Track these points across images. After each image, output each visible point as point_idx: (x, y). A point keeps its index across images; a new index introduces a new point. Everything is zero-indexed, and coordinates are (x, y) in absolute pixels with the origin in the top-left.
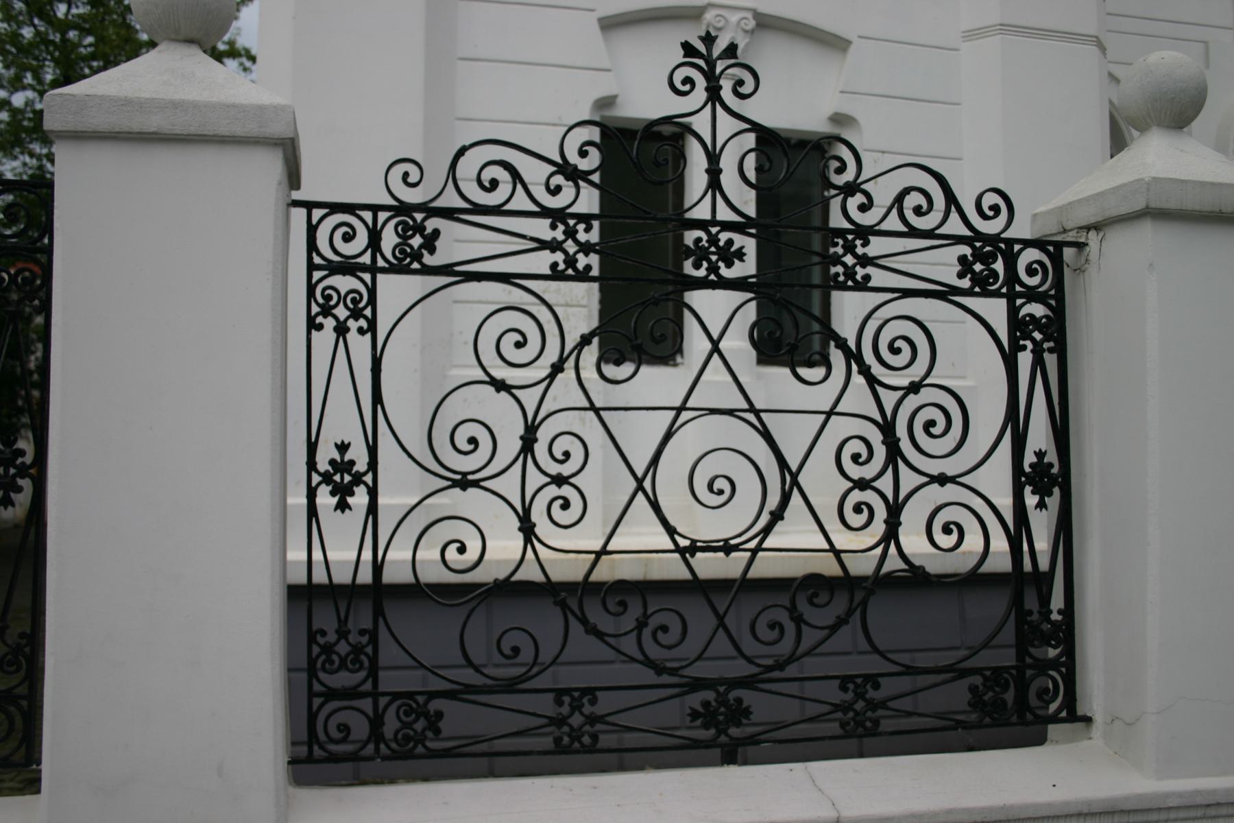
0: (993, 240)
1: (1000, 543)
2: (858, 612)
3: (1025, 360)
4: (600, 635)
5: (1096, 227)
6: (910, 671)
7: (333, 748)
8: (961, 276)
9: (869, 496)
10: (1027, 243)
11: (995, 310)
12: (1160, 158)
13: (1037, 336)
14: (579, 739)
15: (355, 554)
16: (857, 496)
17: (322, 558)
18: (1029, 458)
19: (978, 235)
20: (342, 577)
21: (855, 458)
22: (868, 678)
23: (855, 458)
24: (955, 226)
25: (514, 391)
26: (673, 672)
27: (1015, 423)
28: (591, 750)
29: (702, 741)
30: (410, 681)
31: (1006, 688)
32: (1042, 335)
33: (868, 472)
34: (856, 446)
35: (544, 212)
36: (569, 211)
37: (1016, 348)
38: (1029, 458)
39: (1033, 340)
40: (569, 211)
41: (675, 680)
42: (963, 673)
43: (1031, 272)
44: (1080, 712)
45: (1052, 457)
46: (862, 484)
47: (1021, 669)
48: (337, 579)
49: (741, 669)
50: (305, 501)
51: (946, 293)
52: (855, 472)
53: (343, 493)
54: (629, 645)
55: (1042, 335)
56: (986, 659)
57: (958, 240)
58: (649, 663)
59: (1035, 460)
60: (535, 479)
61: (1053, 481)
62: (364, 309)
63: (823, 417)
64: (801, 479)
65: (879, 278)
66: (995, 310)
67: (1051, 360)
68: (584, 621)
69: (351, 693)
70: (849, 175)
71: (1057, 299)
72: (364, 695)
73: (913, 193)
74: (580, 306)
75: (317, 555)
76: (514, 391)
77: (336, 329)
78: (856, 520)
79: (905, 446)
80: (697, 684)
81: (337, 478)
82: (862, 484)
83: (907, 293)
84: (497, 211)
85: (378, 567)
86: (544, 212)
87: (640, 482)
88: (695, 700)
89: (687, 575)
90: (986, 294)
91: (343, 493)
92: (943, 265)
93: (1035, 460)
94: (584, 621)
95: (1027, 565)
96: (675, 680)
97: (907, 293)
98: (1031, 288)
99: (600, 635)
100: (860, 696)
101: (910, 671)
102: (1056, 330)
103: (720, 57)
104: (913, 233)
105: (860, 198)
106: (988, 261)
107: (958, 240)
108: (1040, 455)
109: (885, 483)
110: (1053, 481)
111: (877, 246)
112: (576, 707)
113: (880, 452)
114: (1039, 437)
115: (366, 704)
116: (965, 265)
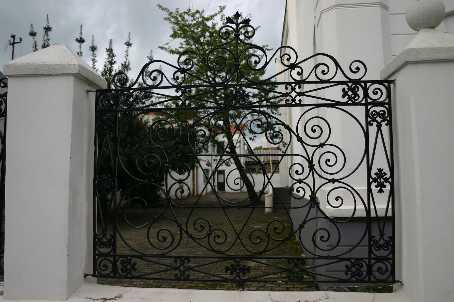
0: (358, 82)
1: (360, 206)
3: (373, 130)
4: (194, 239)
5: (393, 74)
7: (103, 273)
8: (343, 97)
10: (373, 82)
11: (359, 111)
12: (424, 40)
13: (379, 119)
14: (183, 275)
15: (354, 206)
17: (373, 208)
18: (374, 171)
19: (351, 81)
20: (381, 214)
21: (297, 172)
22: (186, 258)
24: (340, 77)
25: (316, 148)
26: (222, 253)
28: (187, 279)
29: (345, 280)
30: (127, 252)
36: (361, 80)
38: (374, 171)
39: (377, 121)
40: (361, 80)
41: (222, 255)
42: (342, 260)
44: (397, 279)
45: (387, 170)
47: (370, 259)
48: (379, 215)
49: (244, 253)
50: (366, 188)
53: (381, 186)
54: (204, 242)
57: (339, 83)
60: (309, 181)
65: (306, 100)
66: (359, 111)
67: (385, 129)
68: (187, 233)
69: (108, 254)
70: (292, 61)
71: (388, 105)
72: (111, 256)
73: (320, 66)
75: (372, 207)
76: (316, 148)
77: (377, 126)
79: (317, 167)
81: (382, 180)
83: (317, 106)
85: (368, 211)
86: (173, 86)
87: (269, 182)
90: (354, 104)
91: (381, 186)
92: (335, 93)
94: (187, 233)
95: (373, 214)
96: (222, 255)
97: (317, 106)
98: (374, 100)
99: (194, 239)
102: (388, 117)
103: (241, 23)
104: (322, 81)
105: (297, 70)
106: (354, 89)
107: (339, 83)
109: (309, 181)
111: (306, 87)
112: (182, 264)
113: (307, 170)
114: (380, 162)
116: (345, 94)
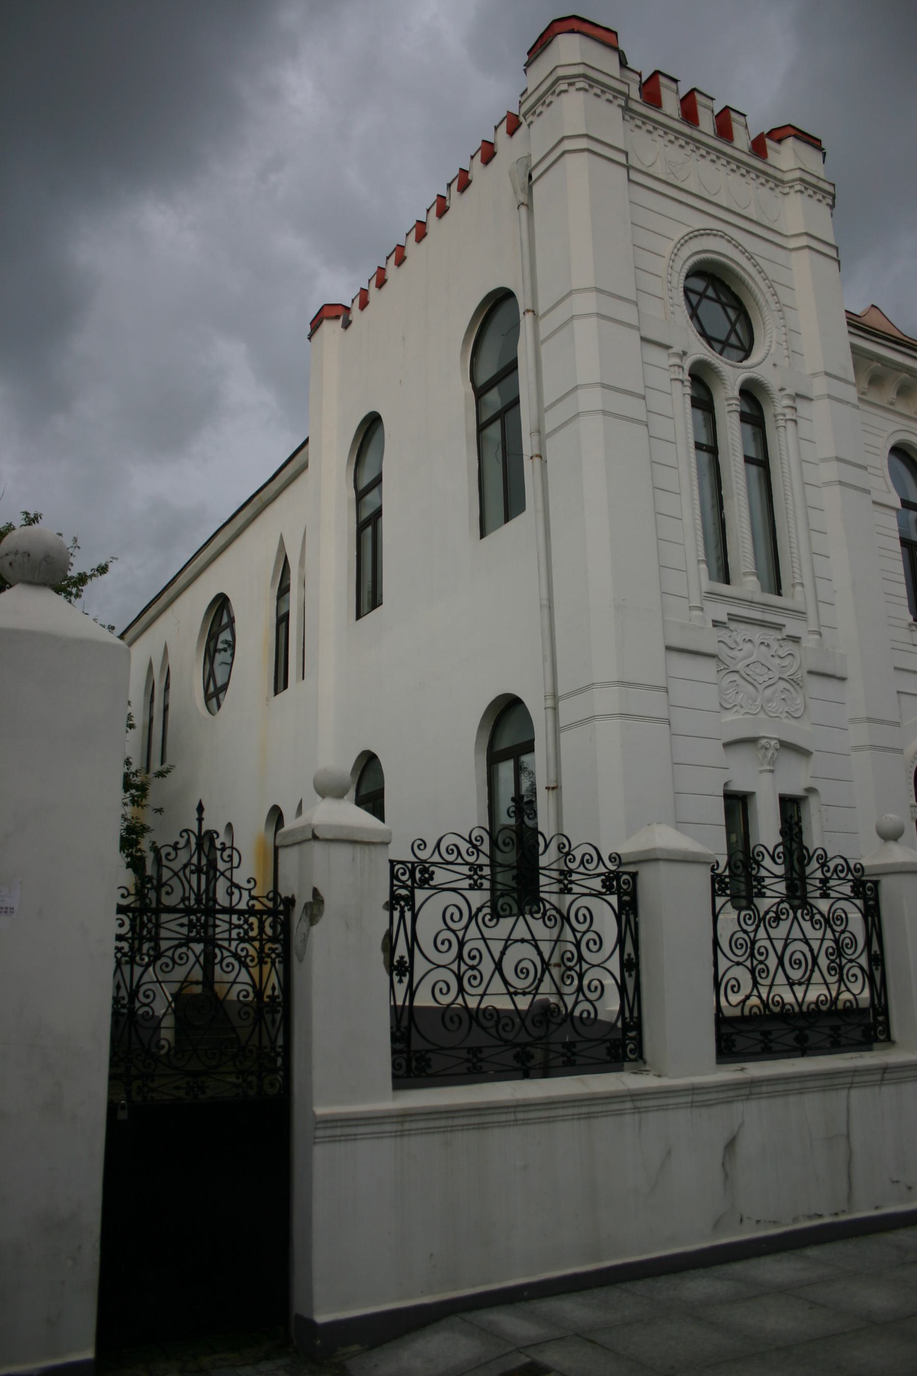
2: (473, 913)
6: (454, 890)
9: (470, 962)
11: (613, 899)
16: (475, 962)
23: (475, 978)
27: (621, 941)
31: (420, 879)
32: (628, 910)
33: (470, 973)
34: (475, 983)
35: (467, 863)
37: (408, 1029)
42: (604, 1041)
43: (624, 883)
46: (473, 968)
51: (598, 895)
52: (475, 973)
55: (628, 910)
56: (426, 893)
58: (501, 1039)
59: (403, 978)
61: (396, 968)
62: (410, 900)
63: (479, 998)
64: (182, 979)
74: (478, 898)
78: (474, 953)
80: (516, 1045)
82: (473, 968)
84: (452, 863)
88: (514, 1051)
89: (512, 1007)
93: (403, 978)
100: (475, 881)
101: (454, 890)
108: (629, 955)
110: (406, 970)
115: (405, 1055)
